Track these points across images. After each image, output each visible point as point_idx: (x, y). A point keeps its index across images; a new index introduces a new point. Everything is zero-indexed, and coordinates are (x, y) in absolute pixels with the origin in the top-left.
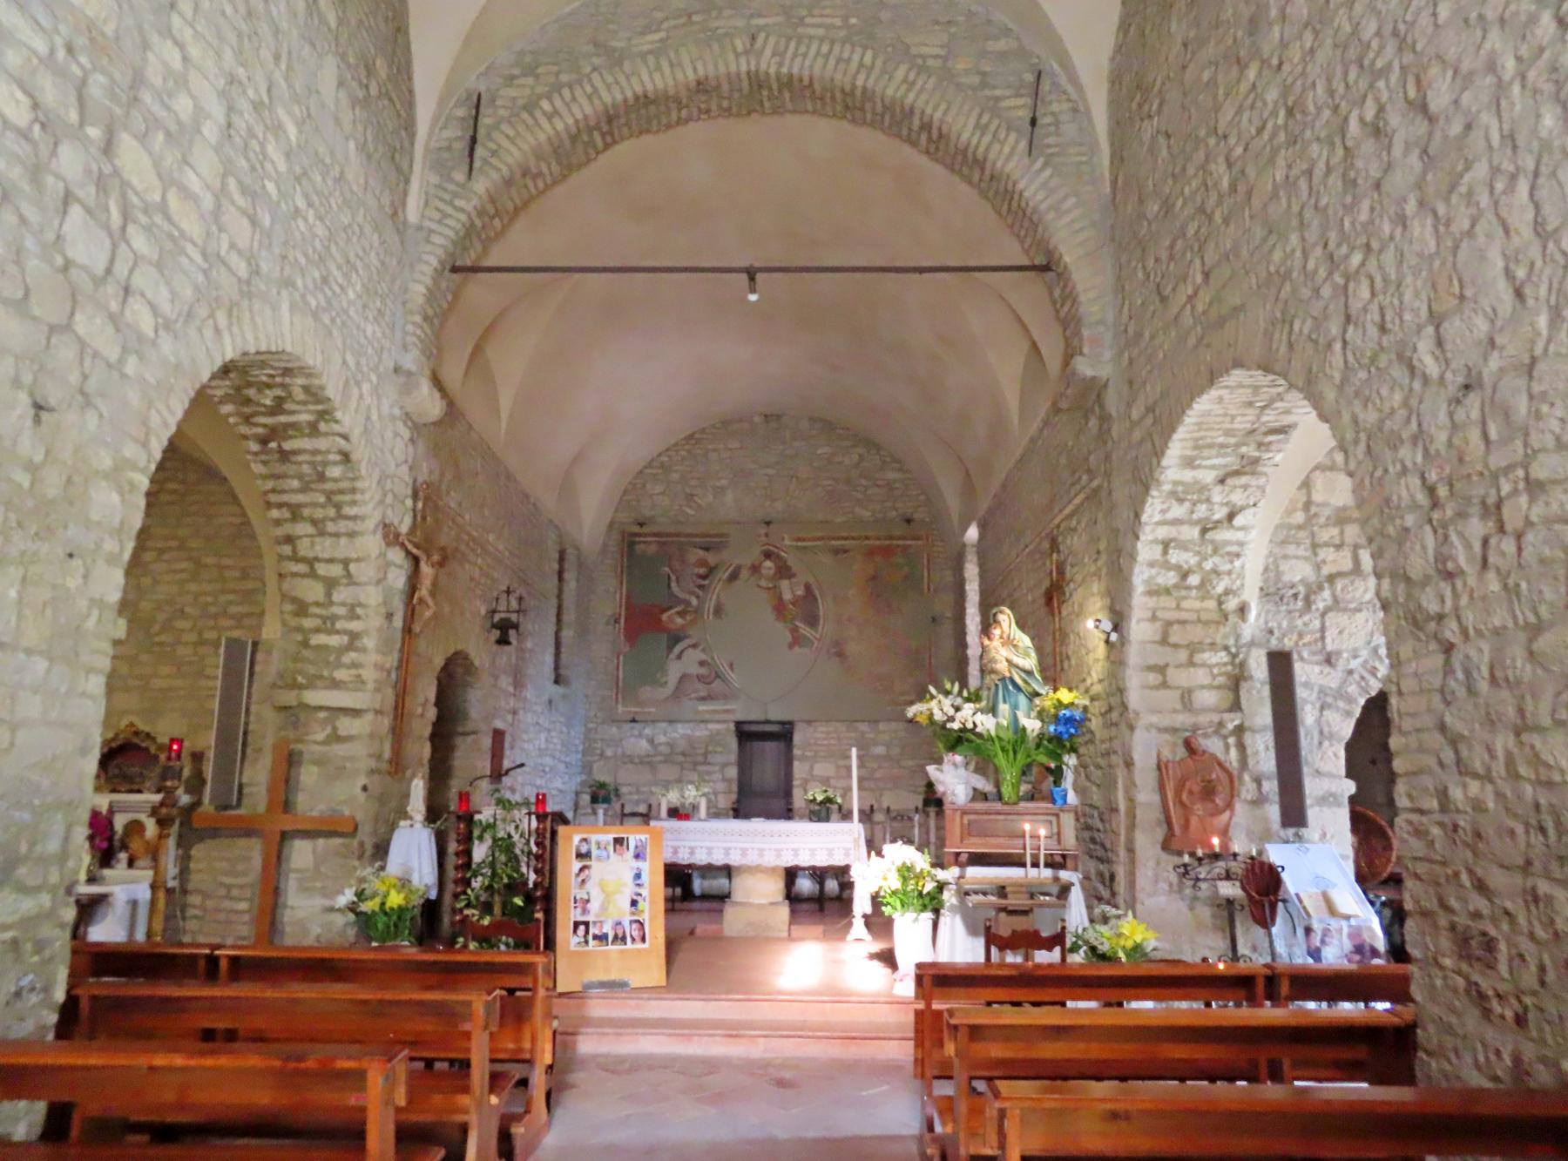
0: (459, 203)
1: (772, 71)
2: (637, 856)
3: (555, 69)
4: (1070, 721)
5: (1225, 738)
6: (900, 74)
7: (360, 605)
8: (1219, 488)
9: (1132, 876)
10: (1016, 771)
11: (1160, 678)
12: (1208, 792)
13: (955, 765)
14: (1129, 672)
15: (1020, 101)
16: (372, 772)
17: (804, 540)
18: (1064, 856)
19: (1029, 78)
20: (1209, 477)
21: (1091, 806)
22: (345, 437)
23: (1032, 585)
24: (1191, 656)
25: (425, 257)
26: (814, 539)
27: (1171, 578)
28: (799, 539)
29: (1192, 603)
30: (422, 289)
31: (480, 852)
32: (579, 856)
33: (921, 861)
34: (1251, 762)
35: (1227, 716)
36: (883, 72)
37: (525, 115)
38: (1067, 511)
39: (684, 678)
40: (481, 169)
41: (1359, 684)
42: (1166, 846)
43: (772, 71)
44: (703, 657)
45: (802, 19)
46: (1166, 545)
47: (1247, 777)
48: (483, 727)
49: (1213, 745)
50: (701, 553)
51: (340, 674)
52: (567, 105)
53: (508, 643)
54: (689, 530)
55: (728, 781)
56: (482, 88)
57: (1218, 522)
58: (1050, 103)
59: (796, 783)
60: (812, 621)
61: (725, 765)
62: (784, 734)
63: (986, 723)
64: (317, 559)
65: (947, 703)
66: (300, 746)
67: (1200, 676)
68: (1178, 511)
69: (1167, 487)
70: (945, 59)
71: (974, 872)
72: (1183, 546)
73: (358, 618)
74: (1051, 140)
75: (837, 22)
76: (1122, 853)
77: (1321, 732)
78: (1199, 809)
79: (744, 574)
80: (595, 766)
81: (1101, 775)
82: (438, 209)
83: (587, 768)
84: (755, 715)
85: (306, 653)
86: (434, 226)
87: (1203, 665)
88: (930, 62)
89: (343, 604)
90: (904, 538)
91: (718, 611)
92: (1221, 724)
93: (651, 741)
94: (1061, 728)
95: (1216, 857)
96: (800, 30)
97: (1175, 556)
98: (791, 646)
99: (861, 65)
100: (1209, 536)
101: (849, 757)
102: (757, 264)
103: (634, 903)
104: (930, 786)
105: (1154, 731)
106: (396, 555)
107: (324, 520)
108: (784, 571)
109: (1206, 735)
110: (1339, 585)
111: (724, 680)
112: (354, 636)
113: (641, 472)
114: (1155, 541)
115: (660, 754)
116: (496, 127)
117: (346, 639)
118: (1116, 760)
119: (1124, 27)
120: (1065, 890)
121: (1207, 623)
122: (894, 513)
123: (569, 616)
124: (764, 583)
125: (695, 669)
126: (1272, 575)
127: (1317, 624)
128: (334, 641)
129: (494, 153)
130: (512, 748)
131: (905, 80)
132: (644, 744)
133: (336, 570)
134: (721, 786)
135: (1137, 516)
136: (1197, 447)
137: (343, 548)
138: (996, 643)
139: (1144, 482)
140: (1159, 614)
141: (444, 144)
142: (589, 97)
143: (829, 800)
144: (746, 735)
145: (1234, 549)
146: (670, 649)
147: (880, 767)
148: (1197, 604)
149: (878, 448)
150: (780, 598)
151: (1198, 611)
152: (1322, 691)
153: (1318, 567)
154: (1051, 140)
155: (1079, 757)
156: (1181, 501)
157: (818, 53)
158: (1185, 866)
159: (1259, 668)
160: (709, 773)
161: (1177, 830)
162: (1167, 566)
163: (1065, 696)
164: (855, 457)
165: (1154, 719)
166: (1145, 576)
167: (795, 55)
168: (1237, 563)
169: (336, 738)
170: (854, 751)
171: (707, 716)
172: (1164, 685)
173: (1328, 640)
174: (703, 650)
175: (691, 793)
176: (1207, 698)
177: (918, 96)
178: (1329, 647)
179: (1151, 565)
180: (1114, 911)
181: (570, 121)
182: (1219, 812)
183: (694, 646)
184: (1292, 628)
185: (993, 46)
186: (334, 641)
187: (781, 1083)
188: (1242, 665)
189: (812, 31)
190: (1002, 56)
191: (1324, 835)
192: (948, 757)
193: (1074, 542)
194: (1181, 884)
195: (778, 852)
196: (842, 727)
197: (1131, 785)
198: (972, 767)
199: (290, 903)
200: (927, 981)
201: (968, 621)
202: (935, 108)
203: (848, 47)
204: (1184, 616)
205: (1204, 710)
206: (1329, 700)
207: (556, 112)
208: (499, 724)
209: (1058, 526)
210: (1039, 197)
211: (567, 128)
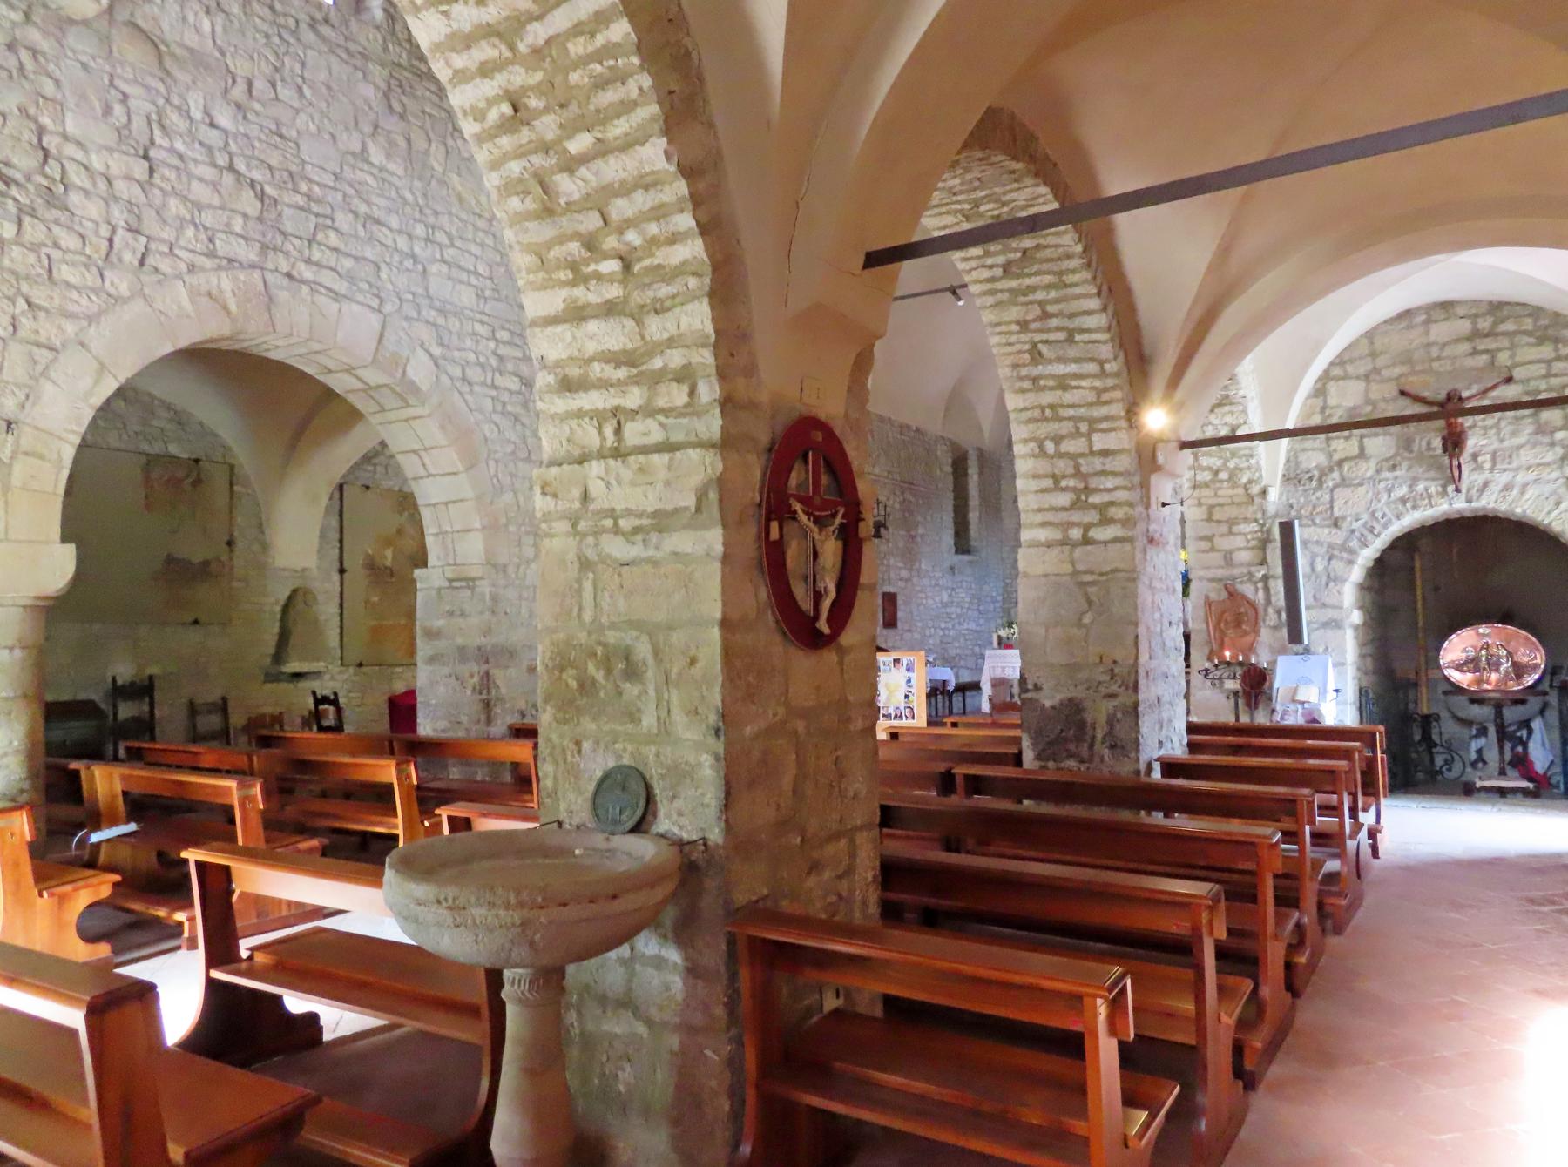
2: (908, 670)
12: (1238, 623)
24: (1230, 528)
27: (1206, 476)
29: (1226, 491)
35: (1253, 569)
41: (1360, 540)
47: (1270, 610)
49: (1247, 590)
67: (1239, 541)
77: (1329, 576)
87: (1240, 534)
92: (1251, 574)
103: (907, 697)
105: (1205, 582)
109: (1242, 582)
110: (1346, 467)
121: (1239, 504)
126: (1293, 464)
127: (1327, 497)
130: (906, 603)
140: (1203, 501)
148: (1230, 492)
152: (1331, 546)
153: (1330, 456)
165: (1202, 573)
168: (1253, 461)
172: (1212, 549)
173: (1336, 509)
176: (1244, 556)
178: (1337, 513)
182: (1246, 633)
184: (1307, 502)
188: (1269, 532)
191: (1327, 649)
204: (1221, 501)
206: (1336, 552)
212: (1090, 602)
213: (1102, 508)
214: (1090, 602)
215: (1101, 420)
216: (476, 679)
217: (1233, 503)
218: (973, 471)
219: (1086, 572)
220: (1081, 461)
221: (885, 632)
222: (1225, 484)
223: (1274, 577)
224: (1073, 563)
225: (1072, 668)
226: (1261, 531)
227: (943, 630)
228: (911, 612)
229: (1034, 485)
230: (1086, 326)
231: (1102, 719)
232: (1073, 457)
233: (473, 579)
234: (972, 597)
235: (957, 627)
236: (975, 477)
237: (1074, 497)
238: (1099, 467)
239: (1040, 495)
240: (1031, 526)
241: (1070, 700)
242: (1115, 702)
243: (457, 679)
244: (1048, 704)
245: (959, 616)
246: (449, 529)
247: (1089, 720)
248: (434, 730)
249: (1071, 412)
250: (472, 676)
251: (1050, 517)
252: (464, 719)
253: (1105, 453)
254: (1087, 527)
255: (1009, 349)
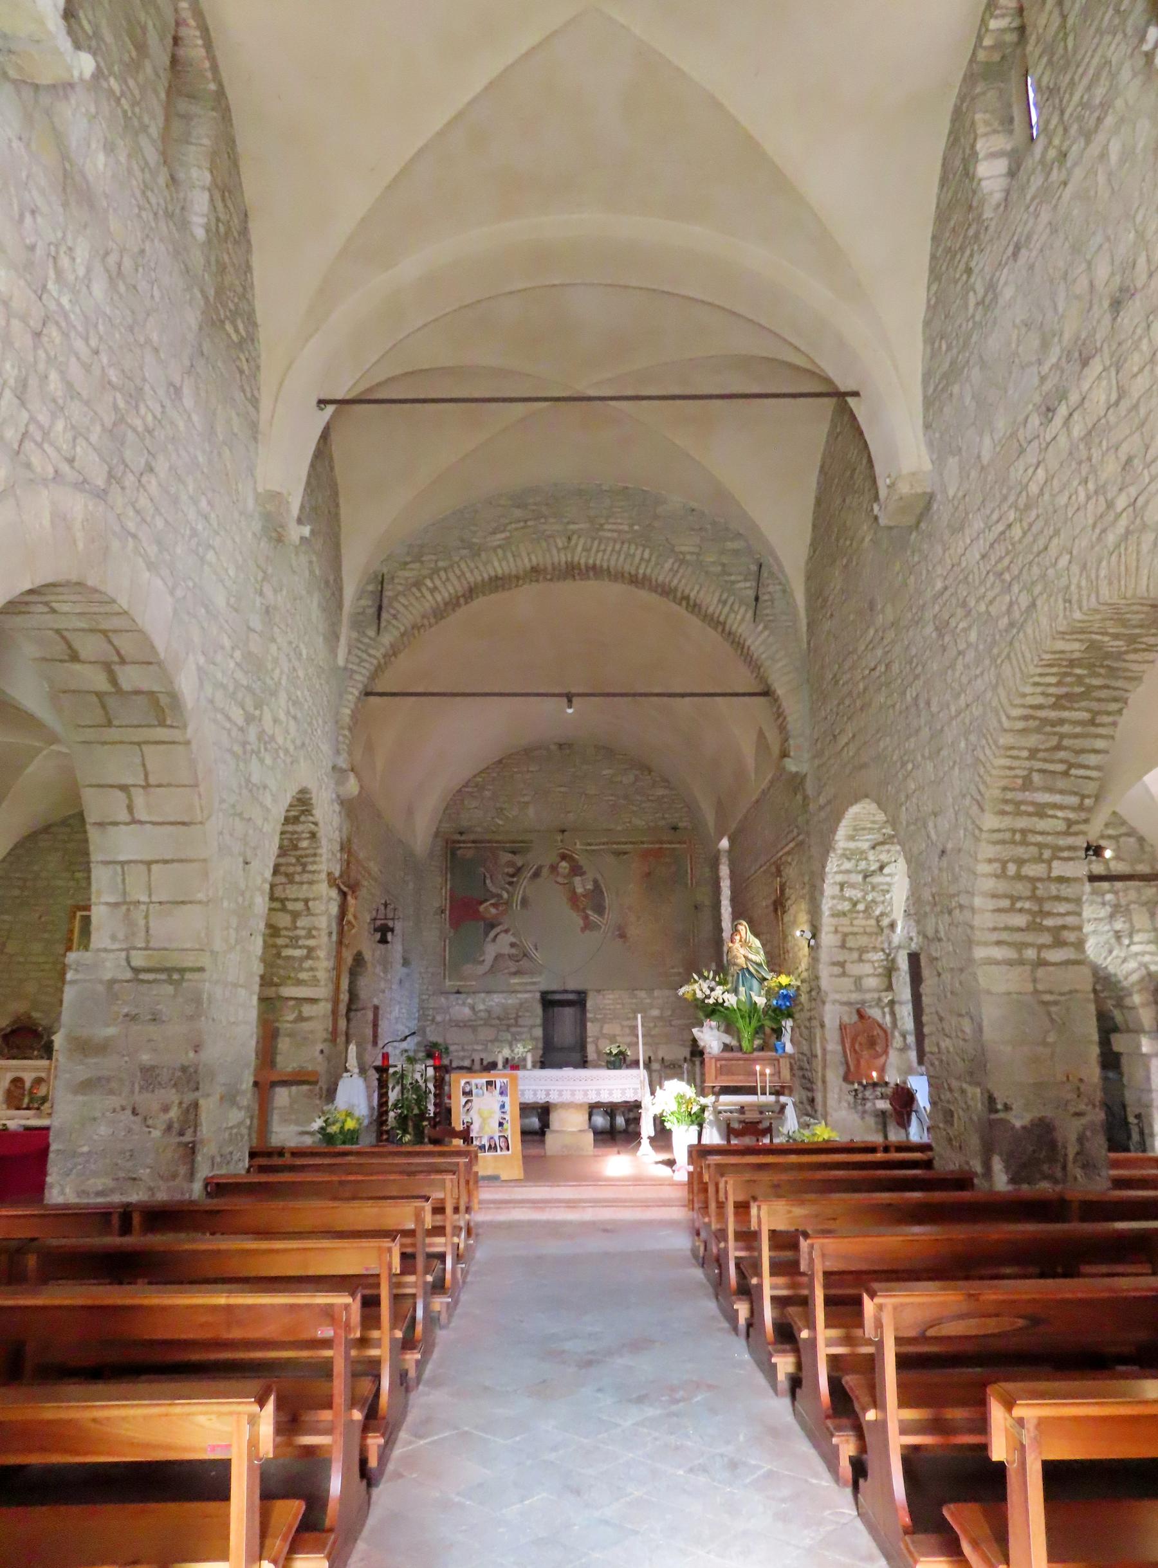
0: (372, 652)
1: (583, 561)
2: (501, 1093)
3: (434, 557)
4: (786, 997)
5: (883, 1008)
6: (667, 566)
7: (315, 928)
8: (872, 852)
9: (825, 1097)
10: (751, 1029)
11: (841, 970)
12: (872, 1043)
13: (711, 1027)
14: (821, 966)
15: (748, 584)
16: (325, 1040)
18: (783, 1087)
19: (754, 568)
20: (865, 846)
21: (802, 1053)
22: (316, 824)
23: (762, 904)
24: (860, 956)
25: (351, 689)
26: (600, 844)
27: (846, 906)
30: (348, 711)
31: (393, 1096)
32: (465, 1093)
33: (689, 1091)
34: (899, 1024)
35: (883, 994)
36: (657, 564)
37: (414, 590)
38: (787, 849)
39: (498, 957)
40: (385, 627)
42: (847, 1078)
43: (583, 561)
44: (513, 940)
45: (602, 525)
46: (842, 886)
47: (897, 1034)
48: (370, 1005)
49: (875, 1013)
51: (303, 976)
52: (444, 583)
54: (500, 838)
55: (533, 1039)
56: (385, 570)
57: (874, 871)
58: (768, 585)
59: (589, 1040)
60: (600, 909)
61: (533, 1026)
62: (579, 1001)
63: (731, 1000)
64: (287, 899)
65: (705, 986)
66: (277, 1024)
67: (867, 969)
68: (848, 865)
69: (839, 852)
70: (698, 554)
71: (724, 1098)
72: (853, 886)
73: (314, 937)
74: (768, 611)
75: (626, 528)
76: (819, 1083)
78: (866, 1054)
79: (545, 872)
80: (428, 1029)
81: (807, 1033)
82: (359, 657)
85: (279, 962)
86: (355, 668)
87: (869, 961)
88: (688, 557)
89: (303, 928)
90: (670, 843)
91: (524, 902)
92: (880, 999)
93: (473, 1008)
94: (780, 1002)
95: (875, 1085)
96: (601, 533)
97: (848, 893)
99: (642, 559)
100: (868, 880)
102: (574, 691)
103: (501, 1124)
104: (695, 1041)
106: (334, 893)
107: (293, 874)
108: (576, 870)
109: (870, 1006)
112: (310, 950)
113: (460, 791)
114: (835, 883)
116: (395, 598)
117: (305, 951)
118: (815, 1023)
119: (814, 545)
120: (783, 1107)
121: (870, 934)
124: (560, 880)
125: (507, 950)
128: (297, 953)
129: (395, 617)
131: (671, 570)
132: (467, 1010)
133: (299, 906)
135: (824, 867)
136: (855, 830)
137: (304, 892)
138: (737, 945)
139: (827, 848)
140: (840, 929)
141: (360, 610)
142: (458, 578)
143: (621, 1053)
144: (549, 1002)
145: (885, 887)
146: (486, 934)
147: (655, 1026)
148: (863, 922)
149: (650, 771)
151: (864, 927)
154: (768, 611)
155: (794, 1021)
156: (849, 859)
157: (613, 550)
158: (856, 1090)
159: (903, 964)
161: (852, 1068)
162: (843, 898)
163: (784, 980)
164: (632, 778)
165: (837, 997)
166: (830, 905)
167: (598, 551)
168: (888, 896)
169: (301, 1018)
170: (639, 1016)
171: (518, 988)
172: (844, 974)
176: (872, 982)
177: (680, 581)
179: (833, 898)
180: (812, 1121)
181: (446, 595)
182: (877, 1056)
183: (506, 931)
185: (730, 545)
186: (297, 953)
187: (605, 1231)
188: (893, 961)
189: (609, 534)
190: (736, 552)
192: (707, 1023)
193: (790, 872)
194: (855, 1102)
195: (586, 1093)
197: (824, 1039)
198: (722, 1028)
199: (274, 1130)
200: (694, 1153)
201: (723, 910)
202: (692, 589)
203: (633, 547)
204: (855, 929)
205: (869, 991)
207: (436, 588)
208: (376, 1001)
209: (780, 858)
210: (761, 649)
211: (443, 599)
212: (1052, 1020)
213: (1057, 931)
214: (1052, 1020)
215: (1062, 849)
216: (174, 1113)
217: (865, 933)
219: (1045, 992)
220: (1039, 885)
222: (861, 915)
223: (901, 1003)
224: (1035, 981)
225: (1039, 1086)
226: (887, 960)
229: (991, 904)
230: (1087, 763)
231: (1073, 1137)
232: (1033, 880)
233: (182, 971)
237: (1030, 918)
238: (1054, 892)
239: (996, 914)
240: (986, 944)
241: (1042, 1120)
242: (1084, 1121)
243: (134, 1112)
244: (1018, 1124)
246: (144, 898)
247: (1059, 1139)
248: (79, 1194)
249: (1039, 838)
250: (166, 1109)
251: (1004, 936)
252: (144, 1173)
253: (1061, 880)
254: (1041, 947)
255: (1008, 773)
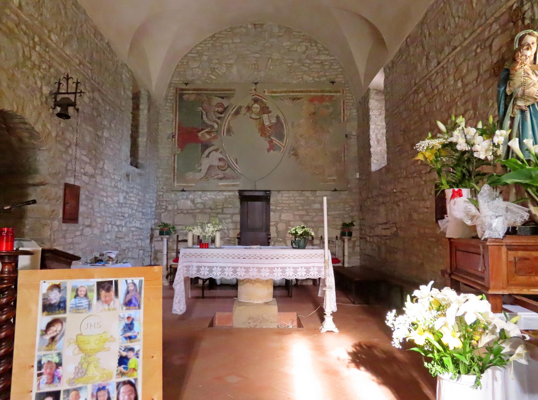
2: (128, 304)
17: (276, 93)
26: (281, 92)
28: (273, 92)
32: (48, 308)
39: (210, 167)
44: (221, 156)
50: (220, 100)
53: (68, 117)
60: (281, 137)
61: (233, 214)
62: (265, 198)
79: (243, 111)
80: (163, 215)
83: (158, 216)
84: (248, 187)
90: (331, 92)
91: (229, 131)
93: (193, 201)
98: (269, 150)
101: (322, 203)
103: (123, 361)
111: (233, 170)
113: (186, 56)
115: (199, 209)
122: (325, 78)
123: (143, 129)
124: (254, 116)
125: (216, 163)
130: (90, 199)
132: (189, 203)
134: (231, 226)
143: (306, 233)
146: (203, 151)
150: (263, 124)
160: (225, 219)
164: (304, 48)
174: (221, 152)
175: (210, 229)
183: (216, 150)
196: (296, 194)
218: (143, 106)
221: (65, 226)
227: (118, 226)
228: (92, 208)
234: (140, 201)
235: (128, 224)
236: (146, 112)
245: (130, 216)
